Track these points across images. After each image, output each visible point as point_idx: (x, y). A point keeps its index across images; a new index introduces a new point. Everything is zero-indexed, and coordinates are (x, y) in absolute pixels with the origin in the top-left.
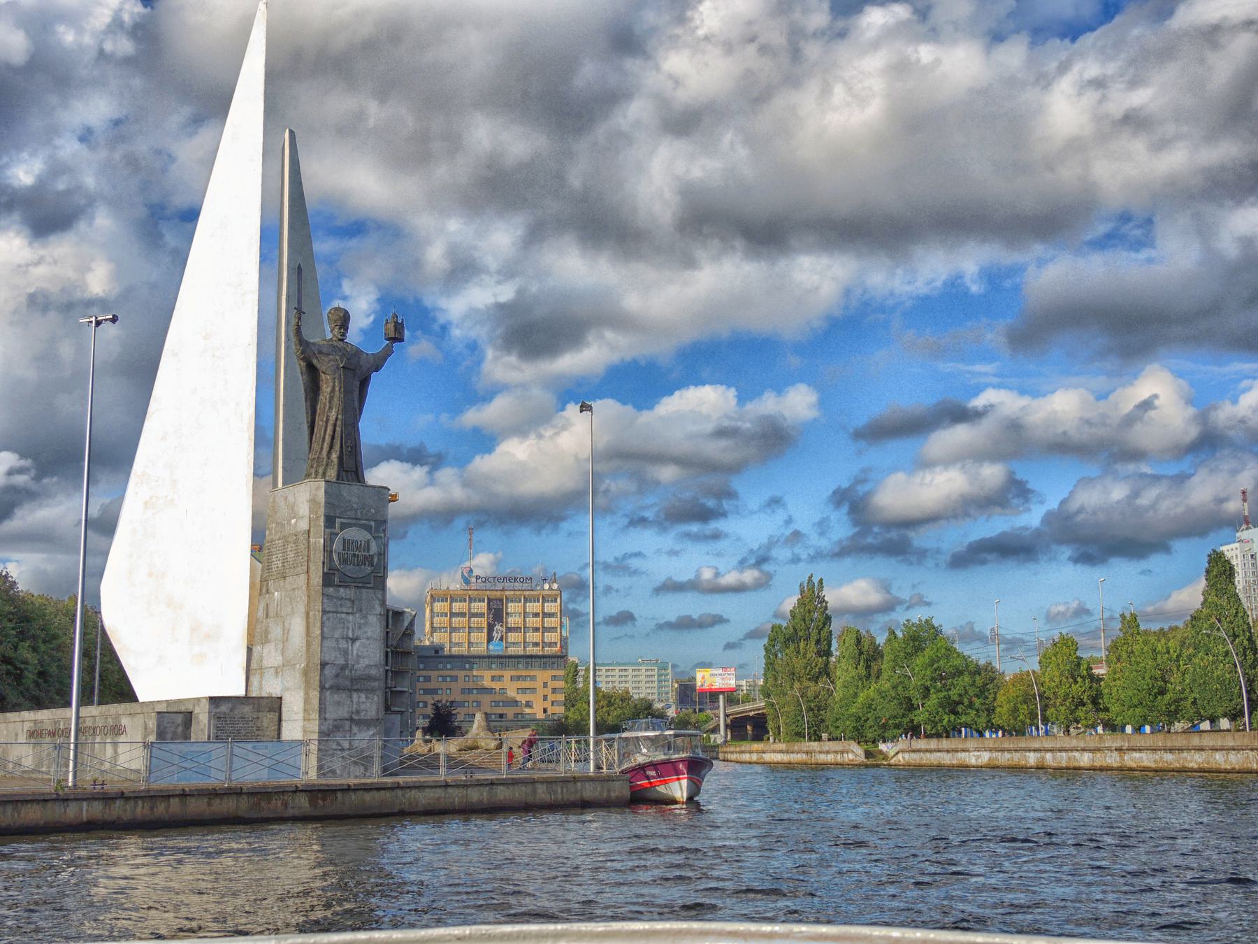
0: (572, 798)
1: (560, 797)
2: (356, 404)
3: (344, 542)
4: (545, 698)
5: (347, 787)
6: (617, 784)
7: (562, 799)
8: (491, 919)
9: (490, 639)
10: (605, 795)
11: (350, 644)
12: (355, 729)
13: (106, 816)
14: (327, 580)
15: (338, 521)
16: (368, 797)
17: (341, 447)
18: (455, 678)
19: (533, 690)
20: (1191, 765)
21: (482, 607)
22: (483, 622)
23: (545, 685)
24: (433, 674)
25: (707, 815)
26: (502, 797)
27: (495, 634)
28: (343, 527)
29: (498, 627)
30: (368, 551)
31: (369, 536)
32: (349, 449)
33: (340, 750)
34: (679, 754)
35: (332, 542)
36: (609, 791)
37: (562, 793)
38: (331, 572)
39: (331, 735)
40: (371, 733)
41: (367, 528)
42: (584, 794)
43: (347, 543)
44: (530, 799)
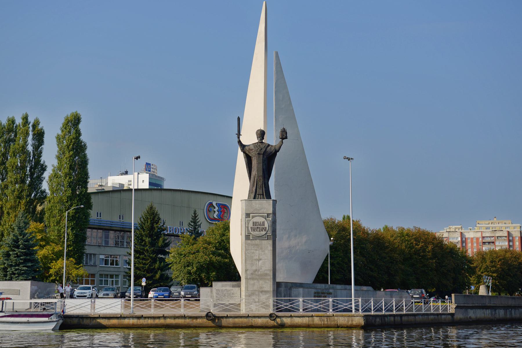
0: (333, 323)
1: (326, 323)
3: (253, 223)
5: (120, 316)
6: (310, 319)
7: (327, 323)
10: (350, 322)
11: (257, 262)
12: (261, 294)
13: (138, 323)
14: (247, 237)
15: (251, 215)
16: (237, 320)
17: (256, 187)
20: (118, 232)
25: (121, 345)
26: (297, 322)
28: (253, 217)
30: (264, 225)
31: (264, 220)
32: (260, 186)
33: (254, 302)
35: (248, 223)
36: (352, 321)
37: (327, 321)
38: (249, 235)
39: (250, 297)
40: (268, 296)
42: (338, 321)
43: (254, 224)
44: (311, 323)
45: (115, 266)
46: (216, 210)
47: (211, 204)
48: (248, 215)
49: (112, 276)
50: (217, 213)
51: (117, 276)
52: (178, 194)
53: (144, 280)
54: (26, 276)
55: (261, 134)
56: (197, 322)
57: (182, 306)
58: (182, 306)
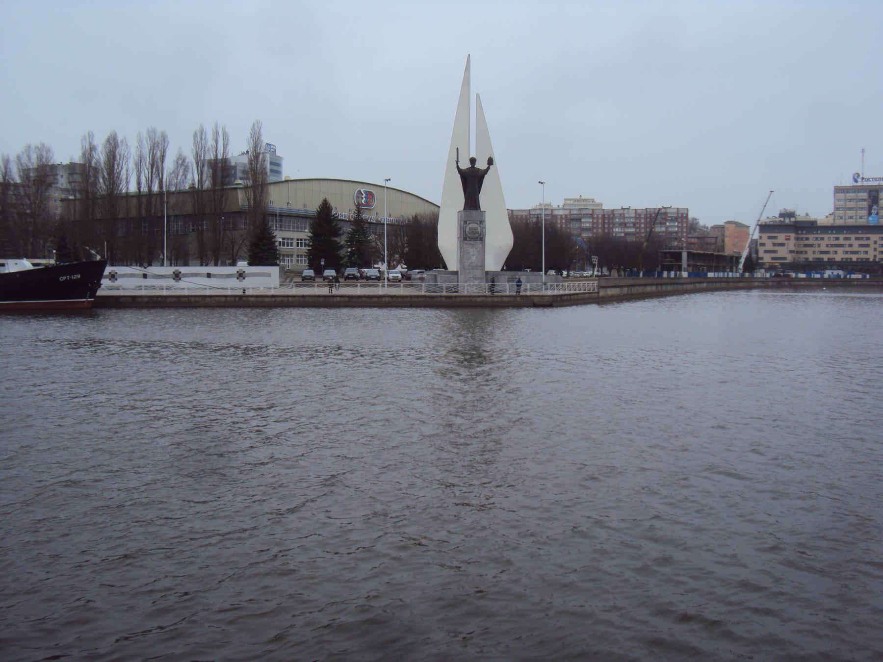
2: (477, 186)
4: (875, 249)
8: (536, 298)
9: (870, 214)
18: (822, 239)
19: (868, 246)
21: (864, 195)
22: (865, 204)
23: (875, 242)
24: (811, 236)
27: (873, 211)
28: (469, 224)
29: (875, 207)
34: (724, 271)
41: (477, 224)
45: (303, 248)
46: (363, 196)
47: (360, 192)
48: (465, 222)
49: (288, 256)
50: (364, 199)
51: (292, 256)
52: (344, 184)
53: (323, 260)
54: (41, 242)
55: (473, 161)
56: (807, 259)
57: (386, 286)
58: (386, 286)
